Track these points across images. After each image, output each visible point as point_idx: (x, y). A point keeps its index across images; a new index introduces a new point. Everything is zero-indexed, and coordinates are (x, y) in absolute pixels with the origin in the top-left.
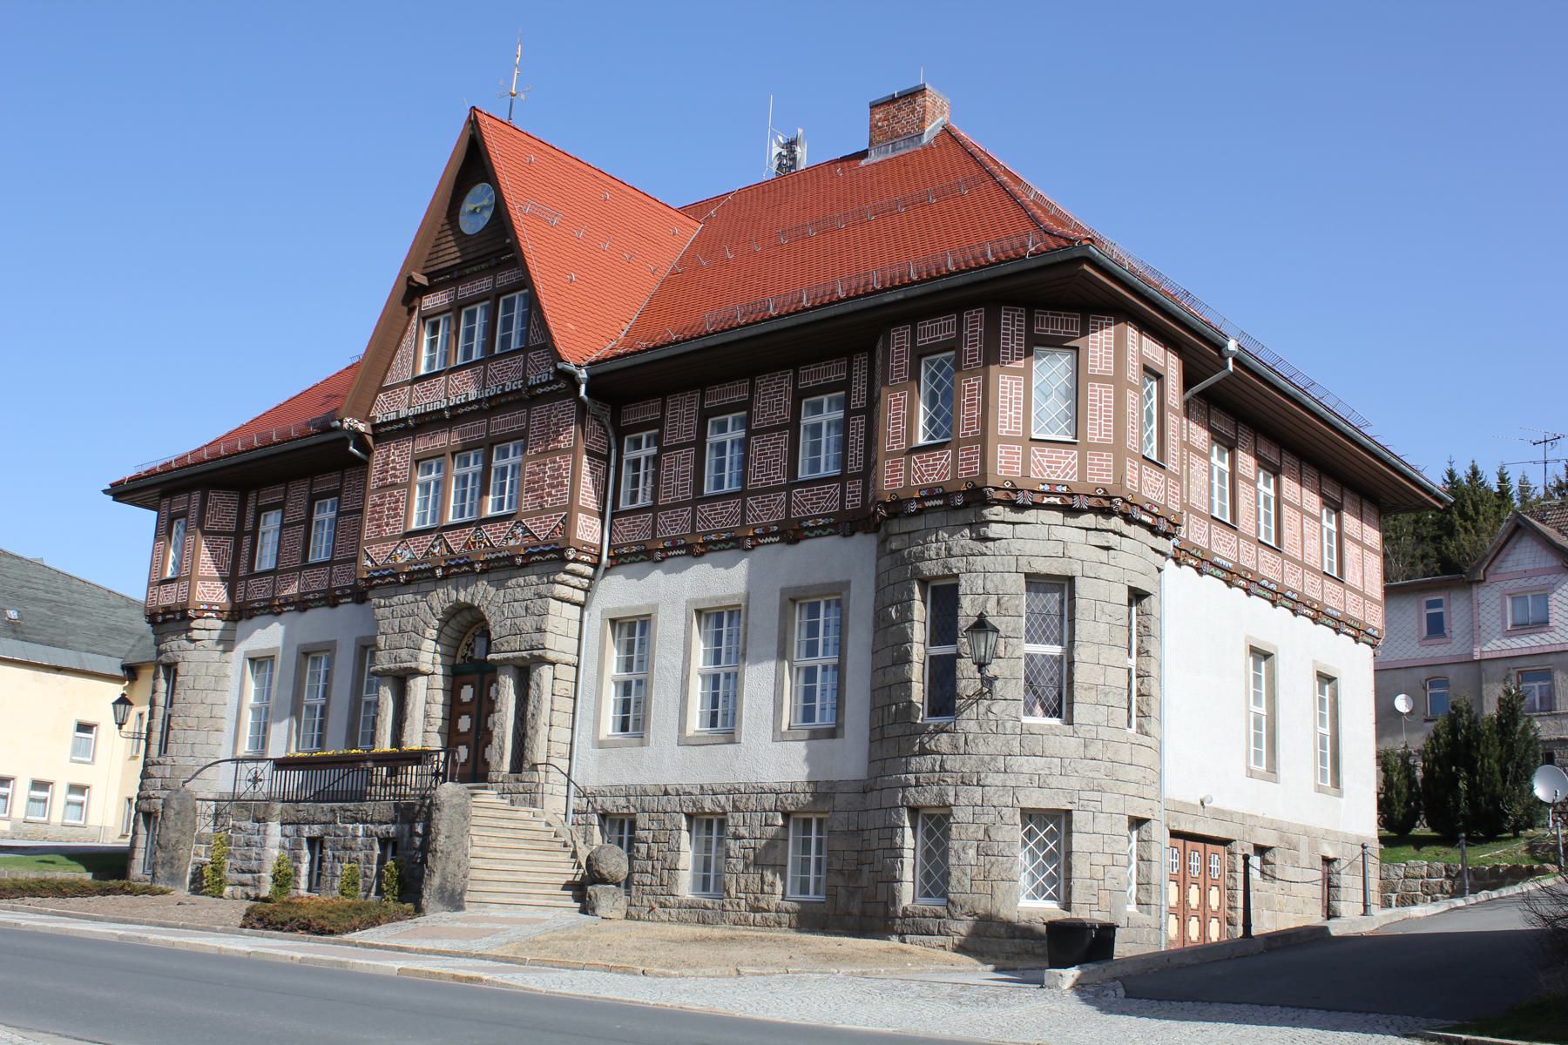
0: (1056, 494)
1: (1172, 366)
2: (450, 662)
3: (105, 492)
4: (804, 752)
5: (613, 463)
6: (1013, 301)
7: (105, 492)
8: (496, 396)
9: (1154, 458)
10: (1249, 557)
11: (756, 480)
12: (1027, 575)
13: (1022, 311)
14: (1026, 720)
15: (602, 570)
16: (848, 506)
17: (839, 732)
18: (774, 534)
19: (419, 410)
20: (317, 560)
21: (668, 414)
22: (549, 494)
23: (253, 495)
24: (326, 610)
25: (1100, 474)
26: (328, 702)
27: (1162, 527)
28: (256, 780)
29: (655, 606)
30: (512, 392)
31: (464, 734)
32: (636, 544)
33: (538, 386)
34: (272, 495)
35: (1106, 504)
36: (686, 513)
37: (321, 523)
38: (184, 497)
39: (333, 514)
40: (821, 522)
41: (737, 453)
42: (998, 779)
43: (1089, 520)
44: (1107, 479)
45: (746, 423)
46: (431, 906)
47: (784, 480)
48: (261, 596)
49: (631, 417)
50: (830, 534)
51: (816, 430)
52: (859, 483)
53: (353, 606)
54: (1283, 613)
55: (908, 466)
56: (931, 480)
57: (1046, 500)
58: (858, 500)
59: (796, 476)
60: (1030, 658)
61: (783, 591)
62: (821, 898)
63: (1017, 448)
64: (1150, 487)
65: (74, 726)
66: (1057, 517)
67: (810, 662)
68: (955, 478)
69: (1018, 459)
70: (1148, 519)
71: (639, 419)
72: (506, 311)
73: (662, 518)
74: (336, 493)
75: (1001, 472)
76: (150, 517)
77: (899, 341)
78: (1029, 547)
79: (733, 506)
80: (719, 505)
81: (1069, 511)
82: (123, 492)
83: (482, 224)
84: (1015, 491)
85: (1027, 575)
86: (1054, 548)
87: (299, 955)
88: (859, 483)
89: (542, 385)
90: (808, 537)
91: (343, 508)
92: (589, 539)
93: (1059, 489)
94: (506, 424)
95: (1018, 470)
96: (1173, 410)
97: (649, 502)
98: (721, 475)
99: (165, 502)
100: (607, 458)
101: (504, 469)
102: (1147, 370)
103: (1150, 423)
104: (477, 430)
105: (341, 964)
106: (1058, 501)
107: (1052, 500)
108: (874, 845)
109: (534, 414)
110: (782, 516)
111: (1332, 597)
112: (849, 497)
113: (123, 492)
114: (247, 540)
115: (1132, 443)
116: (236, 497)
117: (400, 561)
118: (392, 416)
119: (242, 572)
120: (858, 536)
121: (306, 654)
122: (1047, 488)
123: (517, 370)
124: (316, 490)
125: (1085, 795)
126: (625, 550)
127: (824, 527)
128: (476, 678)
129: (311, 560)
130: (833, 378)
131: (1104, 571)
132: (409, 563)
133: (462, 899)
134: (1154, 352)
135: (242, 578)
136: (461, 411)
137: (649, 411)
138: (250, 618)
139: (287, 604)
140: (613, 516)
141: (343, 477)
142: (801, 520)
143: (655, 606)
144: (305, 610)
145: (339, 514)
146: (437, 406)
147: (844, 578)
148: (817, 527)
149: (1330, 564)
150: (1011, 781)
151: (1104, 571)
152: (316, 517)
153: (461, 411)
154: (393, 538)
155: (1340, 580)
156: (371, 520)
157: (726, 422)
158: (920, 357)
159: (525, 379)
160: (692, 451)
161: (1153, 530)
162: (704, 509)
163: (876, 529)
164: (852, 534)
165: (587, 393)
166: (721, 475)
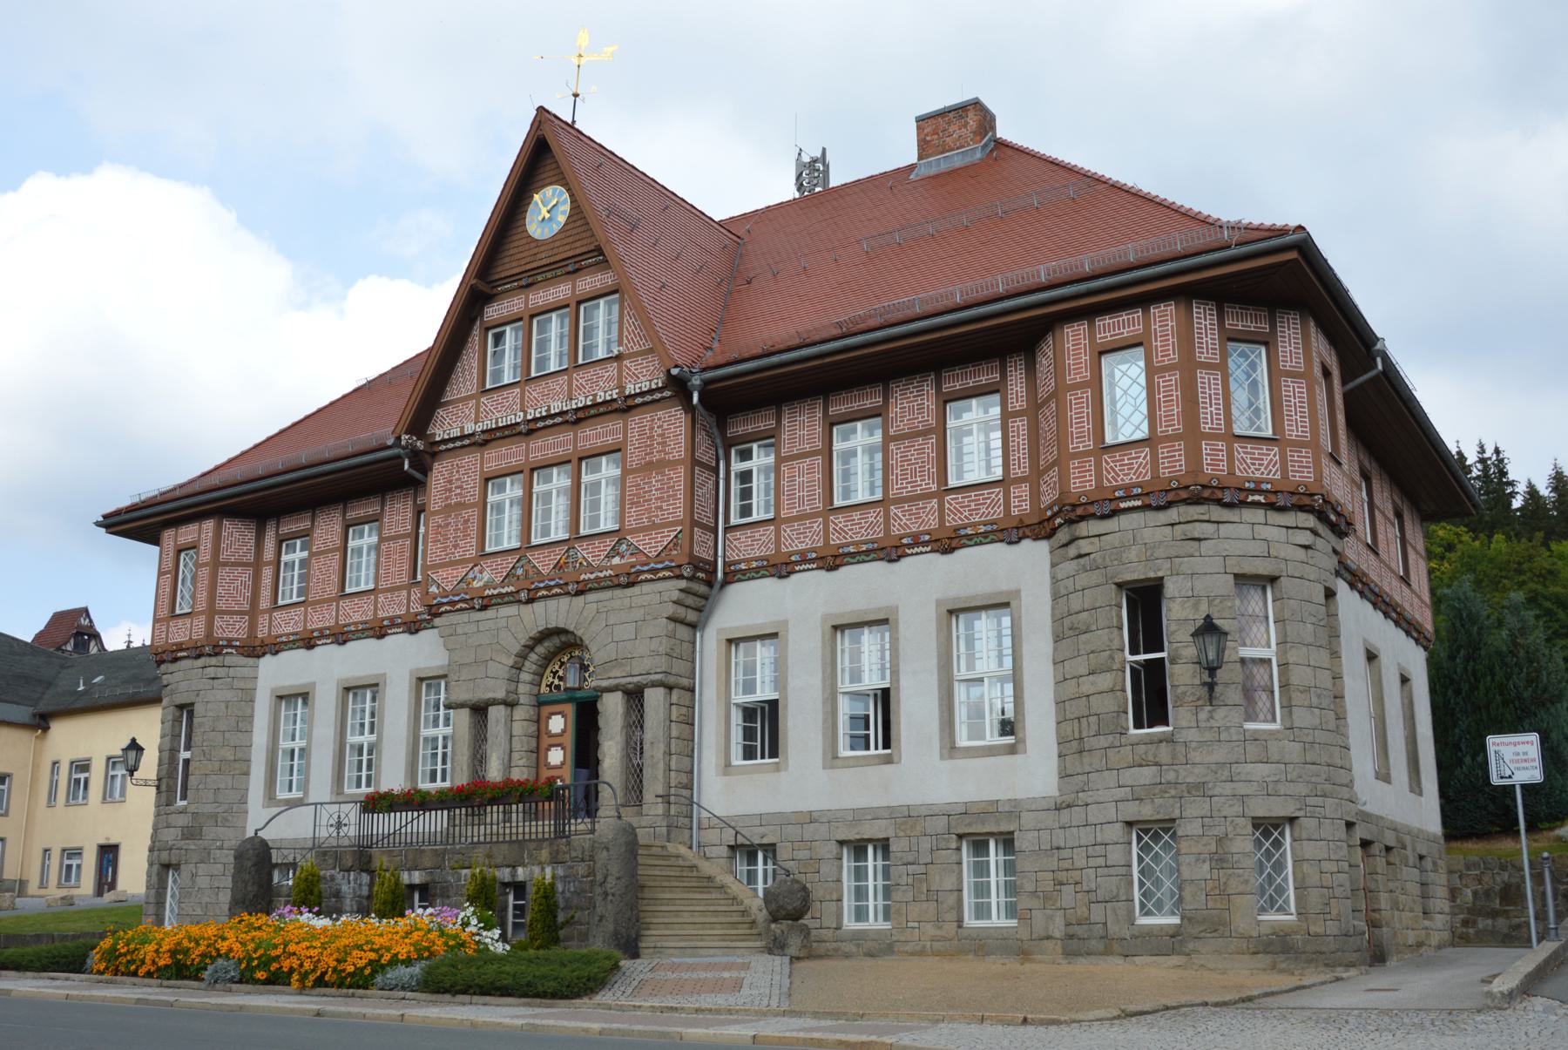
3: (98, 524)
5: (722, 475)
7: (98, 524)
8: (586, 407)
11: (899, 488)
12: (1236, 576)
13: (1212, 305)
14: (1250, 726)
15: (717, 586)
16: (1015, 512)
17: (1020, 747)
20: (971, 478)
28: (339, 825)
29: (786, 622)
30: (605, 402)
33: (636, 395)
36: (817, 525)
38: (193, 527)
39: (375, 539)
40: (982, 529)
41: (373, 556)
42: (1228, 788)
44: (1308, 476)
47: (934, 487)
48: (290, 630)
49: (738, 428)
50: (763, 576)
51: (359, 551)
52: (1025, 487)
53: (406, 636)
55: (1098, 465)
56: (1132, 478)
57: (1250, 499)
59: (832, 503)
63: (1221, 445)
66: (1259, 515)
69: (1223, 456)
71: (750, 428)
72: (496, 344)
73: (787, 531)
74: (305, 534)
85: (1236, 576)
86: (1257, 548)
87: (596, 1026)
88: (1025, 487)
90: (740, 580)
91: (386, 533)
93: (1264, 486)
94: (598, 436)
97: (371, 586)
100: (716, 470)
104: (586, 438)
105: (664, 1035)
106: (1261, 499)
107: (1257, 498)
109: (631, 425)
112: (1014, 502)
114: (267, 572)
117: (476, 584)
118: (456, 433)
119: (264, 603)
120: (1026, 543)
121: (347, 689)
122: (1252, 486)
123: (611, 379)
126: (743, 566)
129: (280, 602)
130: (984, 379)
132: (486, 587)
133: (637, 946)
135: (264, 612)
138: (277, 653)
140: (727, 529)
142: (956, 530)
145: (381, 540)
146: (511, 419)
147: (1013, 586)
148: (859, 553)
150: (1242, 789)
152: (285, 558)
154: (462, 562)
159: (621, 387)
160: (819, 460)
162: (839, 520)
165: (411, 466)
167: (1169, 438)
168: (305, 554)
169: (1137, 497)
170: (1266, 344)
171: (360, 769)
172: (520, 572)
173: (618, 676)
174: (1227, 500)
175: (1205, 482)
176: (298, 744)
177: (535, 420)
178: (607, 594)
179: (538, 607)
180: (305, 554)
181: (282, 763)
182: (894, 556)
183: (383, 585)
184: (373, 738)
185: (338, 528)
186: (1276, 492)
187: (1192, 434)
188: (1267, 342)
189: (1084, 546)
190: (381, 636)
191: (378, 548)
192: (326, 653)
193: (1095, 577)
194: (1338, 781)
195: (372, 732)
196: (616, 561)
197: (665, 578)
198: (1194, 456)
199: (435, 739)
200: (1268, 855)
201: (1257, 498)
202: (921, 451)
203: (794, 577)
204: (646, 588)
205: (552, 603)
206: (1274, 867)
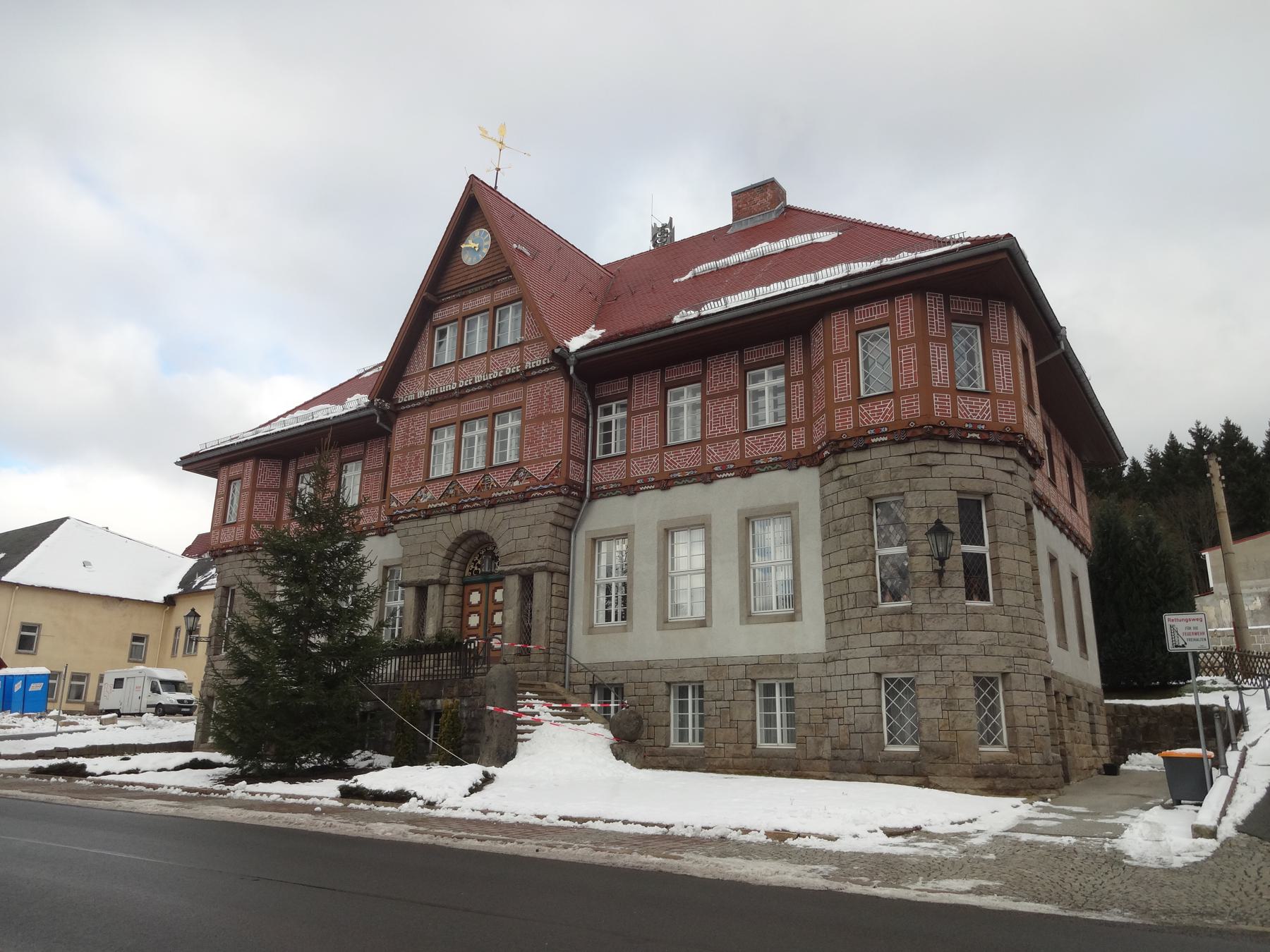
0: (977, 431)
2: (461, 574)
3: (177, 463)
6: (935, 289)
7: (177, 463)
8: (498, 378)
13: (940, 296)
14: (969, 603)
16: (795, 447)
17: (798, 616)
18: (730, 471)
19: (433, 391)
21: (635, 388)
22: (547, 447)
23: (292, 462)
24: (658, 493)
30: (511, 375)
31: (474, 628)
32: (613, 483)
33: (532, 369)
34: (356, 450)
35: (1012, 438)
36: (655, 459)
37: (759, 394)
38: (240, 465)
40: (771, 460)
42: (954, 649)
46: (486, 758)
49: (605, 390)
50: (779, 469)
52: (802, 431)
58: (803, 443)
60: (964, 555)
61: (740, 512)
62: (698, 745)
65: (130, 638)
66: (975, 449)
67: (609, 580)
68: (898, 419)
69: (948, 404)
71: (610, 393)
74: (626, 395)
75: (937, 414)
76: (213, 482)
78: (957, 471)
79: (782, 434)
80: (682, 451)
81: (984, 442)
82: (196, 463)
83: (481, 257)
86: (975, 472)
88: (802, 431)
89: (536, 368)
92: (577, 480)
93: (979, 427)
94: (506, 398)
98: (767, 412)
99: (223, 470)
101: (472, 439)
106: (977, 436)
107: (974, 435)
108: (842, 702)
110: (737, 456)
112: (794, 440)
113: (196, 463)
116: (280, 464)
118: (412, 397)
120: (803, 470)
123: (515, 358)
124: (344, 456)
125: (1018, 660)
127: (773, 464)
128: (483, 587)
130: (692, 374)
131: (1011, 489)
136: (468, 391)
137: (620, 386)
139: (369, 530)
140: (593, 462)
141: (705, 368)
143: (797, 504)
144: (385, 534)
146: (449, 388)
150: (965, 650)
151: (1011, 489)
153: (468, 391)
156: (396, 472)
157: (610, 408)
158: (858, 332)
160: (657, 413)
162: (670, 455)
163: (820, 463)
164: (798, 468)
166: (767, 412)
172: (451, 492)
173: (515, 564)
174: (952, 436)
177: (464, 388)
178: (511, 507)
179: (464, 516)
188: (982, 323)
189: (846, 471)
191: (628, 421)
193: (853, 493)
196: (516, 483)
197: (549, 495)
198: (927, 404)
200: (987, 720)
201: (974, 435)
202: (728, 406)
203: (640, 495)
204: (536, 502)
205: (473, 514)
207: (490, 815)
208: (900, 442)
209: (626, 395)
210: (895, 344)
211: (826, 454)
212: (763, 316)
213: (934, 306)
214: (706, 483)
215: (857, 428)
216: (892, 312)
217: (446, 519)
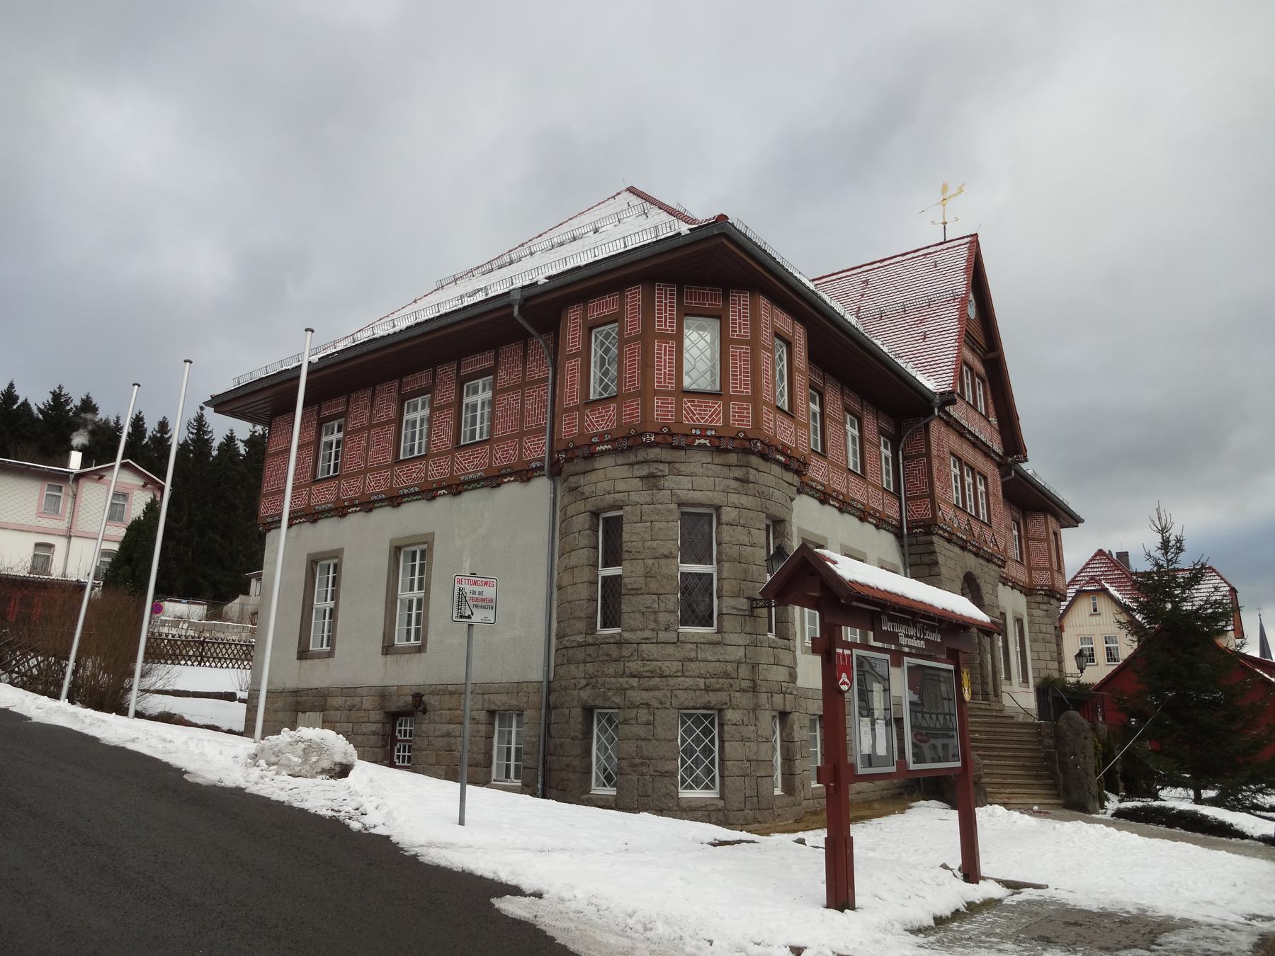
0: (706, 437)
1: (799, 336)
3: (11, 386)
4: (999, 810)
7: (11, 386)
9: (786, 408)
10: (838, 483)
18: (356, 506)
25: (741, 419)
26: (337, 605)
27: (796, 466)
35: (747, 444)
43: (733, 458)
45: (493, 386)
50: (483, 487)
54: (868, 528)
64: (785, 433)
68: (620, 426)
69: (672, 408)
70: (782, 459)
74: (492, 371)
77: (574, 318)
84: (672, 435)
95: (672, 417)
96: (800, 371)
98: (414, 438)
102: (778, 335)
103: (782, 381)
107: (702, 441)
111: (858, 492)
115: (766, 395)
122: (698, 432)
134: (784, 322)
137: (423, 378)
141: (726, 298)
149: (816, 441)
155: (862, 476)
161: (786, 467)
167: (631, 395)
168: (341, 435)
169: (607, 442)
170: (719, 317)
171: (409, 623)
174: (676, 443)
175: (657, 430)
176: (417, 594)
180: (341, 435)
181: (400, 614)
182: (494, 484)
183: (498, 434)
184: (422, 594)
185: (393, 406)
186: (719, 438)
187: (646, 393)
188: (719, 316)
190: (344, 515)
191: (492, 403)
192: (851, 521)
194: (667, 673)
195: (420, 588)
198: (647, 408)
199: (411, 602)
200: (698, 741)
201: (702, 441)
206: (693, 752)
207: (1027, 894)
208: (623, 451)
209: (344, 415)
210: (622, 342)
211: (566, 462)
212: (385, 352)
213: (665, 300)
214: (523, 481)
215: (581, 434)
216: (622, 305)
217: (957, 550)
